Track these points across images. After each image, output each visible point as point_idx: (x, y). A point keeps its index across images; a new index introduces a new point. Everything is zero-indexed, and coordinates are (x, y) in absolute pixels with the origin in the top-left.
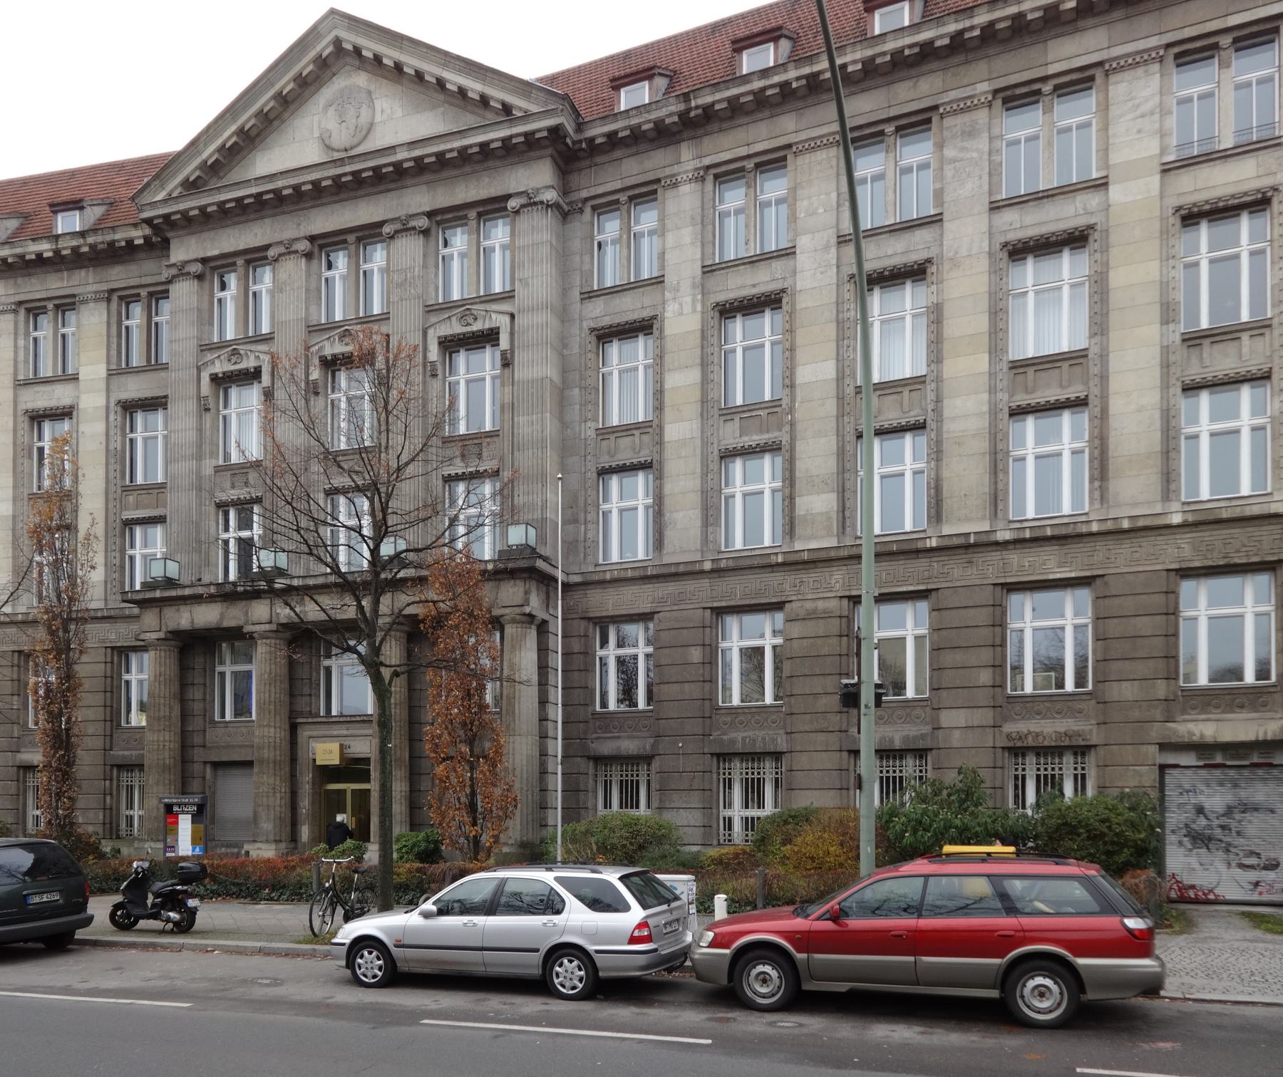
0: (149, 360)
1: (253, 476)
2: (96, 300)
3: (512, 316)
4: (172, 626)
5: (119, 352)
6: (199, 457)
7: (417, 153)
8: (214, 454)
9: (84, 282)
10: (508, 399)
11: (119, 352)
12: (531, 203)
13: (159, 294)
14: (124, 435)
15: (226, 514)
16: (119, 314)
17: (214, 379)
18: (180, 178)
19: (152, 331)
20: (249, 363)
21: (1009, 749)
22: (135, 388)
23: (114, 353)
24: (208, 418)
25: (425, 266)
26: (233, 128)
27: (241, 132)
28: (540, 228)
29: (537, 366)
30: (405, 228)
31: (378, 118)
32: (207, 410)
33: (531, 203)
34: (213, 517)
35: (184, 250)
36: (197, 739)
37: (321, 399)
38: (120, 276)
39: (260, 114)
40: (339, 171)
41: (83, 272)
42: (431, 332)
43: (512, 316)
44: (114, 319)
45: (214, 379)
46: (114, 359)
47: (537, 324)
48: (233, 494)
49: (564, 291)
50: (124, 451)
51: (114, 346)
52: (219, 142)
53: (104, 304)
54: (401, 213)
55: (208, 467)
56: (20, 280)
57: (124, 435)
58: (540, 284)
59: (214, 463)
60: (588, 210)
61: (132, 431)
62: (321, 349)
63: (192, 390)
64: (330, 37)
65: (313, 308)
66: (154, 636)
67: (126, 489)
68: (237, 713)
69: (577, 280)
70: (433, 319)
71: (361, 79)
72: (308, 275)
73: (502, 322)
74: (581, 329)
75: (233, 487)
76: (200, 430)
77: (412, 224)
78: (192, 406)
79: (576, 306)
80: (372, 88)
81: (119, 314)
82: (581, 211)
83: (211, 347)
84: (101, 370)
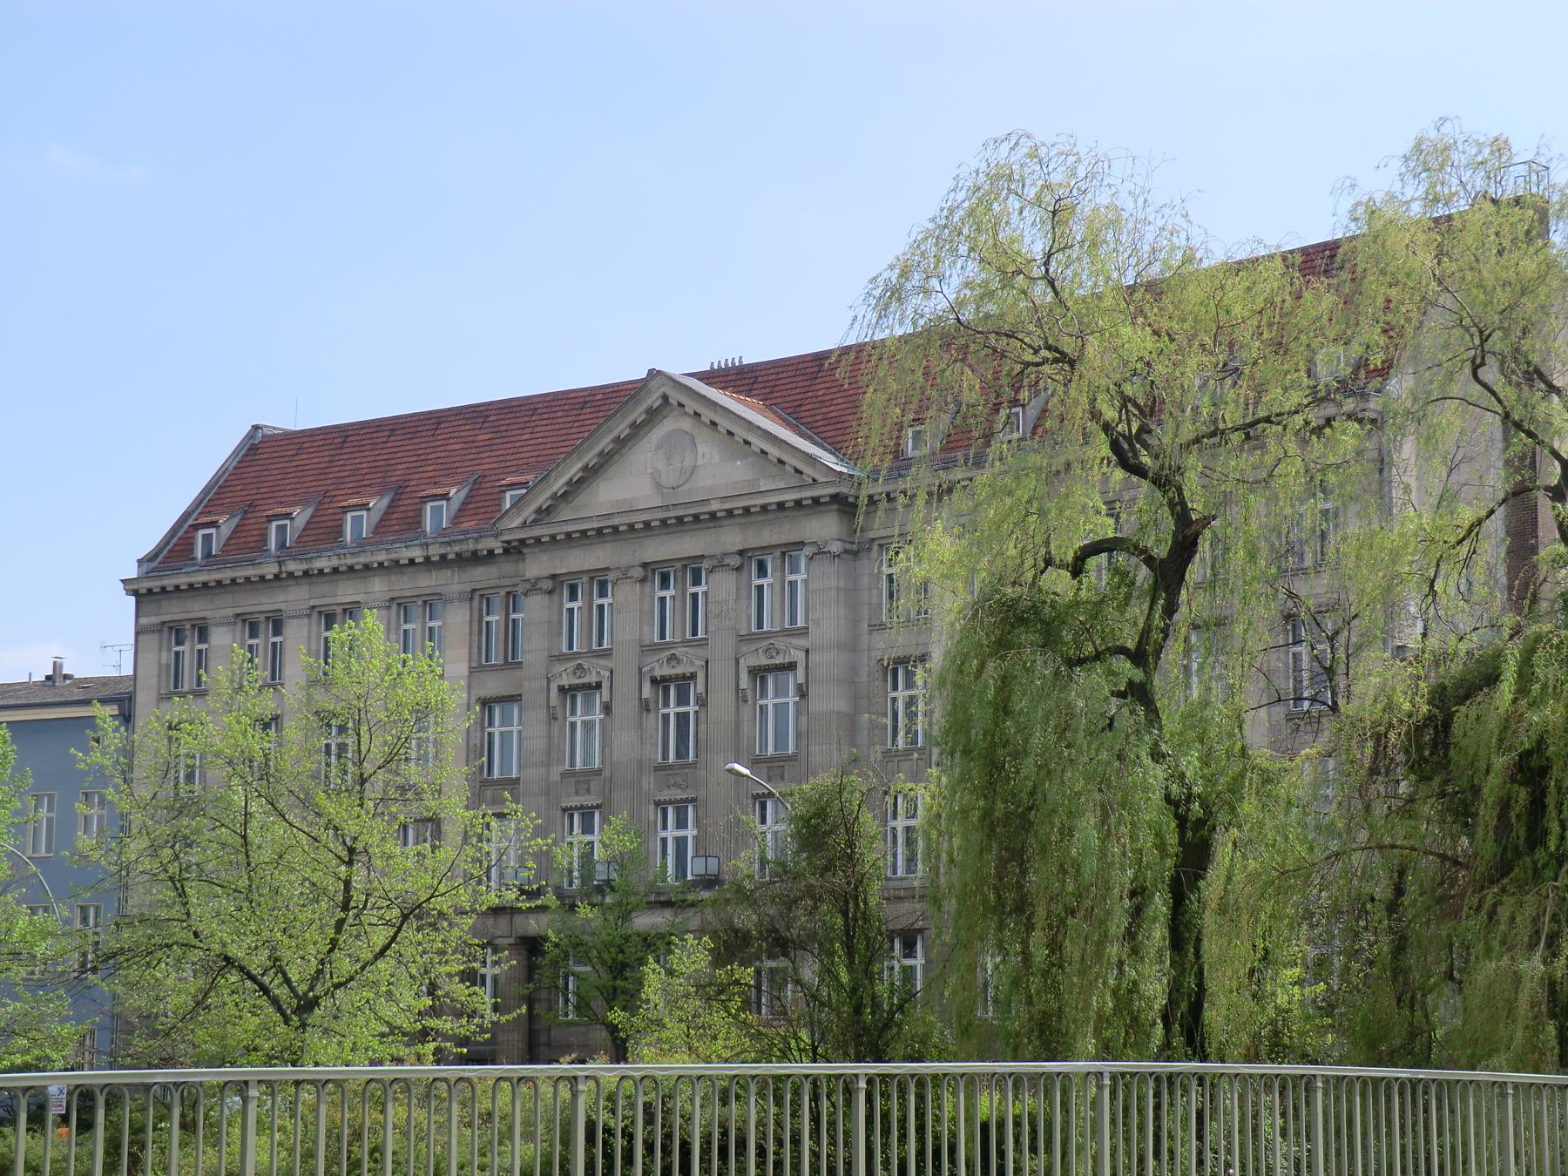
0: (506, 658)
1: (595, 785)
2: (460, 600)
3: (807, 652)
4: (521, 932)
5: (480, 649)
6: (548, 765)
7: (728, 506)
8: (561, 761)
9: (452, 582)
10: (804, 728)
11: (480, 649)
12: (820, 552)
13: (512, 600)
14: (483, 730)
15: (571, 816)
16: (481, 610)
17: (562, 689)
18: (534, 506)
19: (512, 628)
20: (591, 678)
21: (1509, 800)
22: (493, 686)
23: (475, 650)
24: (556, 727)
25: (738, 599)
26: (579, 465)
27: (585, 468)
28: (829, 577)
29: (829, 700)
30: (719, 565)
31: (700, 462)
32: (556, 719)
33: (820, 552)
34: (559, 822)
35: (537, 566)
36: (543, 1039)
37: (652, 715)
38: (481, 575)
39: (601, 454)
40: (665, 515)
41: (449, 572)
42: (742, 661)
43: (807, 652)
44: (476, 617)
45: (562, 689)
46: (475, 656)
47: (827, 661)
48: (574, 801)
49: (856, 622)
50: (482, 746)
51: (475, 644)
52: (567, 477)
53: (467, 605)
54: (718, 550)
55: (555, 773)
56: (393, 578)
57: (483, 730)
58: (827, 623)
59: (561, 769)
60: (875, 548)
61: (490, 725)
62: (653, 669)
63: (543, 702)
64: (659, 393)
65: (646, 629)
66: (506, 941)
67: (485, 783)
68: (678, 755)
69: (865, 613)
70: (745, 649)
71: (686, 424)
72: (642, 596)
73: (799, 657)
74: (869, 658)
75: (577, 793)
76: (549, 737)
77: (727, 561)
78: (542, 715)
79: (865, 639)
80: (695, 433)
81: (481, 610)
82: (869, 549)
83: (562, 658)
84: (463, 669)
